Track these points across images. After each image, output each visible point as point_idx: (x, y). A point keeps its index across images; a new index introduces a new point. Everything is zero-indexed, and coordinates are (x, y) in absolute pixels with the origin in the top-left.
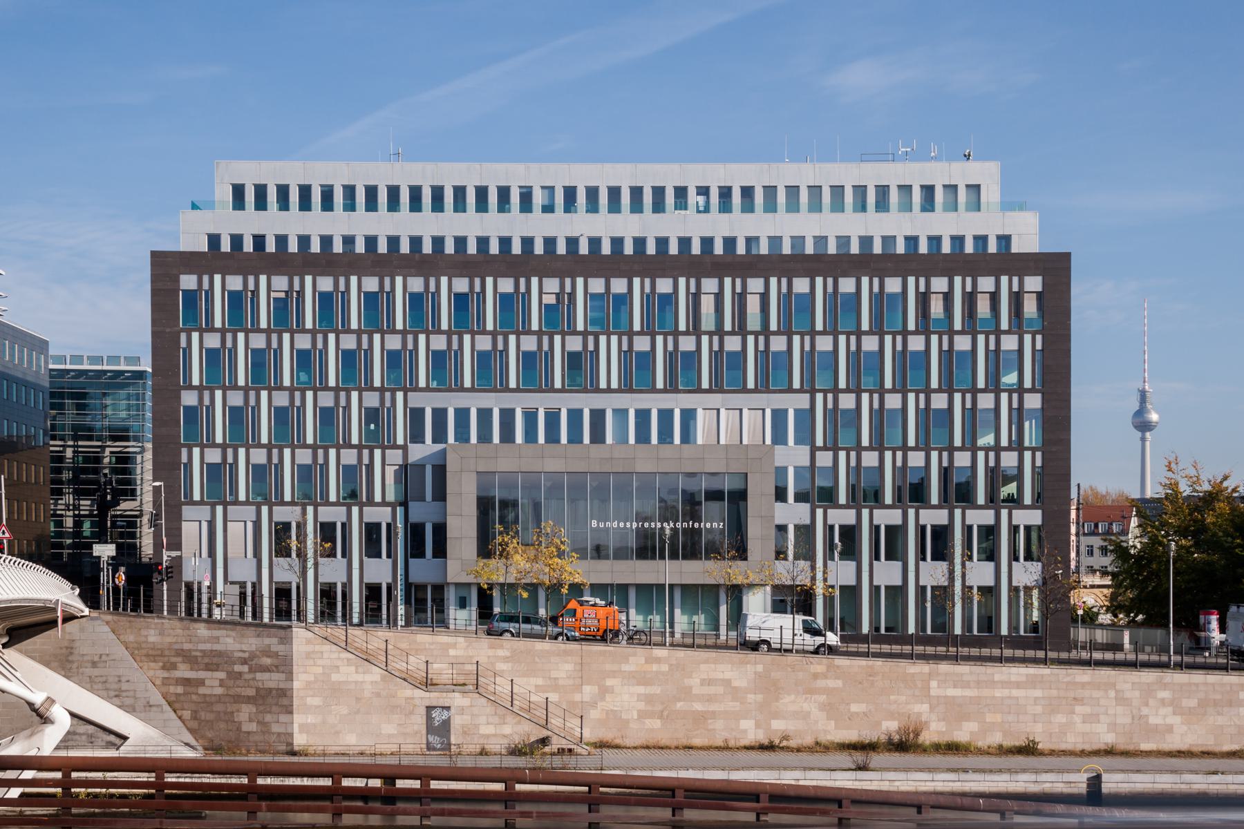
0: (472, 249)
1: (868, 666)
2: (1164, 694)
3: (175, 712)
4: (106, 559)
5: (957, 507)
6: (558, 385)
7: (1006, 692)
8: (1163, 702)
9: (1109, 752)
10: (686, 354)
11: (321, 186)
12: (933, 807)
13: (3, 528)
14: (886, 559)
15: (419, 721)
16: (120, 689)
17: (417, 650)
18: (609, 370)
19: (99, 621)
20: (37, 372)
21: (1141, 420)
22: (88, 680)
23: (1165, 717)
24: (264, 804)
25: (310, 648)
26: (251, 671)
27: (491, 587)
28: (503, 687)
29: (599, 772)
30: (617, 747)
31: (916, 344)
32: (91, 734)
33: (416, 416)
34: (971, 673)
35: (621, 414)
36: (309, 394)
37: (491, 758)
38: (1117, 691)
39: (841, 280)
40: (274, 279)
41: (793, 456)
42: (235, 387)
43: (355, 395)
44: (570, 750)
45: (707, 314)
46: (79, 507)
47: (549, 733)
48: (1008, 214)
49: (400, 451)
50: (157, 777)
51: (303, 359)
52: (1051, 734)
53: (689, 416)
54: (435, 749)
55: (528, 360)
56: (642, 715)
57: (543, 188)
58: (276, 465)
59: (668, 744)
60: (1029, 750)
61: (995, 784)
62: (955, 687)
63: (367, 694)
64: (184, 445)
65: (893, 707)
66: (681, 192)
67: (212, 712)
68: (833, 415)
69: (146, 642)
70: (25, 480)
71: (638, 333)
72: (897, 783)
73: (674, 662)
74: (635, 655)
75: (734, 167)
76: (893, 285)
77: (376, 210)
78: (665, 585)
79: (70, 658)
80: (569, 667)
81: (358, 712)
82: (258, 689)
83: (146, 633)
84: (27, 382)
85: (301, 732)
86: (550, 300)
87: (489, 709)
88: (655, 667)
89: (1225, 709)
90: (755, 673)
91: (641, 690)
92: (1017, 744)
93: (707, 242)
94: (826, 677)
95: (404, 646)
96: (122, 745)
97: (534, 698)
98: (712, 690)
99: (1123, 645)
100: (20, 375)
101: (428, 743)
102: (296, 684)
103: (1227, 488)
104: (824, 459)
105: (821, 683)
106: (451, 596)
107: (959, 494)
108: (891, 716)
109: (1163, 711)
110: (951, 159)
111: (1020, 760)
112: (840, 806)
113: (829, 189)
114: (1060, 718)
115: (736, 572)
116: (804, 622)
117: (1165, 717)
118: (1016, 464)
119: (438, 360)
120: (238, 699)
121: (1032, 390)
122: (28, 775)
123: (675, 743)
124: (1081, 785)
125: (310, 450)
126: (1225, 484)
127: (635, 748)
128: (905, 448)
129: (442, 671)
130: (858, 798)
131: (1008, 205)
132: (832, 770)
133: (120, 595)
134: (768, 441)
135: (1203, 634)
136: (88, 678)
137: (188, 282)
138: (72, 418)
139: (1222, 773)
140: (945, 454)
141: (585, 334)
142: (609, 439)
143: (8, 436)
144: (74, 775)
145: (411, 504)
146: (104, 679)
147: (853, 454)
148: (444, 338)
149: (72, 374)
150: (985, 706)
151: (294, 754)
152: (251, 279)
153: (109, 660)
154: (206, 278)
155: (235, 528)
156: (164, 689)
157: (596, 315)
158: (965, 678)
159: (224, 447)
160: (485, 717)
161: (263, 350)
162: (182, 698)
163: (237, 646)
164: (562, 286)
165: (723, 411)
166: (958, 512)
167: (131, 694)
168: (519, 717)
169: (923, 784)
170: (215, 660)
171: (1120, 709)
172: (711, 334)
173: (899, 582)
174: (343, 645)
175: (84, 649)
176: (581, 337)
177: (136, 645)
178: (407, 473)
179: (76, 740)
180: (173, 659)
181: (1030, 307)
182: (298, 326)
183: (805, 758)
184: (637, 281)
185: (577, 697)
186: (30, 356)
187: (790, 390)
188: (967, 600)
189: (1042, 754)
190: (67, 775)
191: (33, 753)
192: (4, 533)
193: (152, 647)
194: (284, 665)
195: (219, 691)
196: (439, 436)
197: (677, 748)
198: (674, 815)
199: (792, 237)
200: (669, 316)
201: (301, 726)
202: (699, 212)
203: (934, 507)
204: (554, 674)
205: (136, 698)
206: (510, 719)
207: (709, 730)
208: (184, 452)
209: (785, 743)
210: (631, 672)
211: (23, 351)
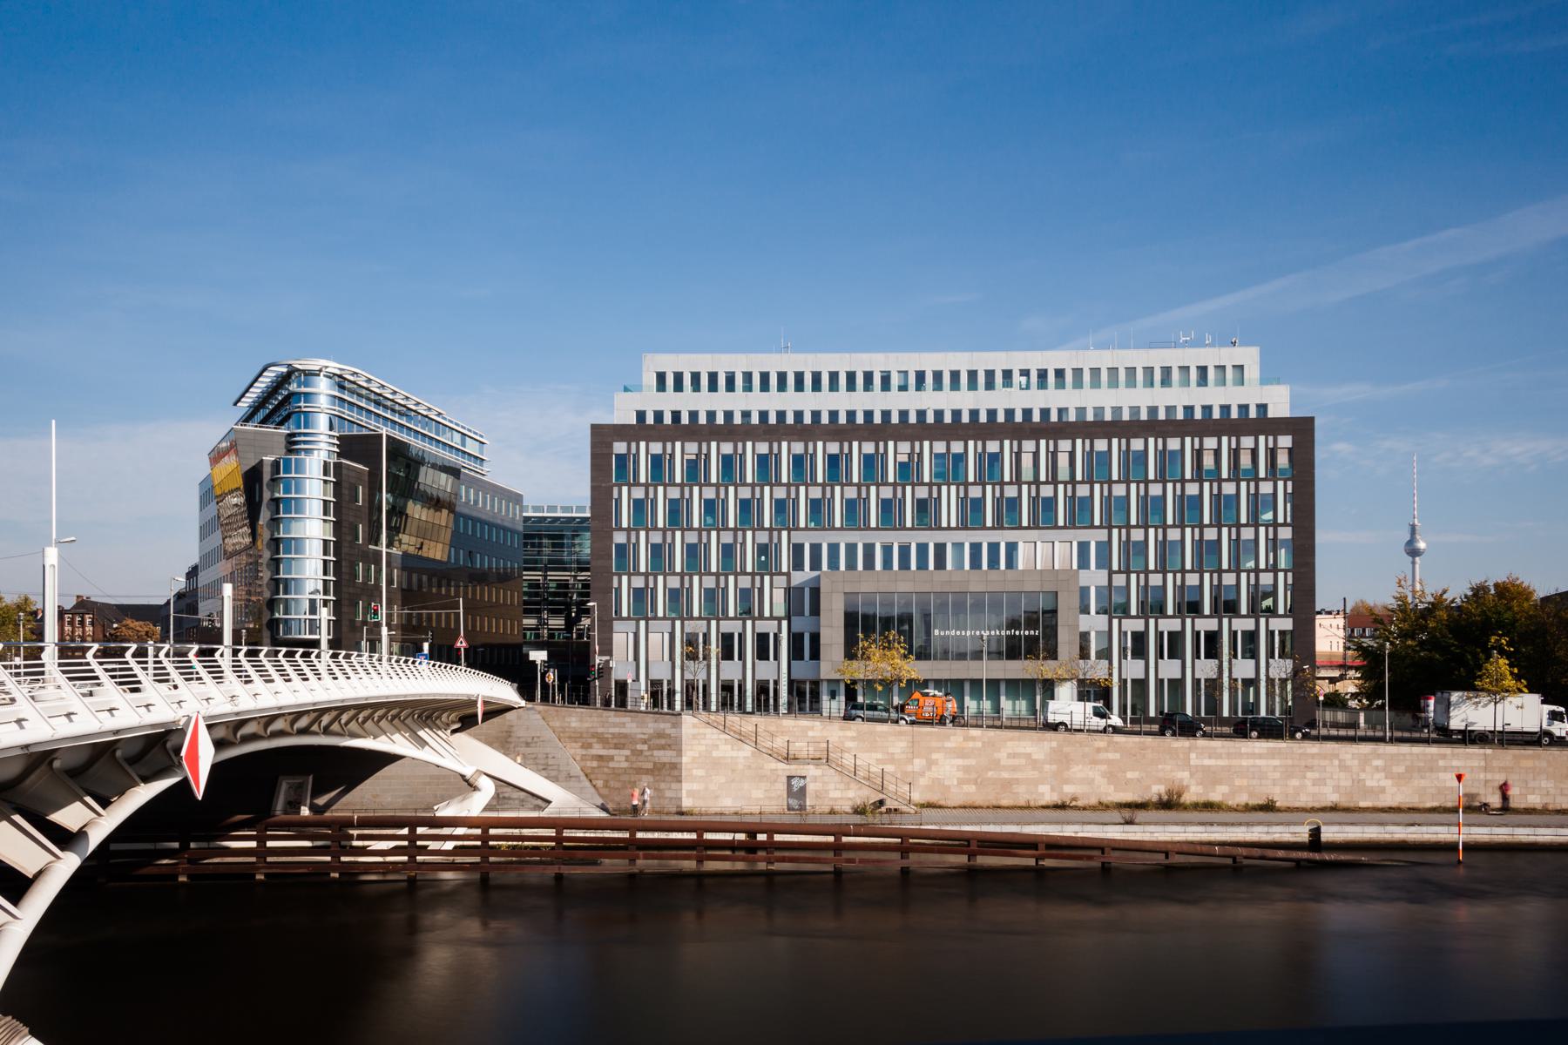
0: (842, 420)
1: (1140, 742)
2: (1378, 763)
3: (591, 781)
5: (1225, 617)
6: (909, 524)
7: (1251, 762)
8: (1377, 769)
9: (1334, 809)
10: (1046, 500)
11: (726, 373)
12: (1178, 853)
14: (1169, 658)
15: (781, 787)
17: (783, 732)
18: (949, 511)
20: (513, 519)
21: (1411, 548)
23: (1379, 780)
24: (641, 853)
25: (695, 731)
26: (649, 749)
27: (854, 682)
28: (848, 761)
29: (918, 827)
30: (940, 807)
31: (1192, 489)
33: (797, 550)
34: (1223, 747)
35: (959, 546)
36: (714, 534)
37: (838, 817)
38: (1340, 761)
39: (988, 443)
40: (687, 445)
41: (1094, 578)
42: (656, 529)
43: (749, 534)
44: (896, 810)
45: (1027, 468)
47: (884, 797)
48: (1265, 387)
49: (785, 577)
50: (630, 835)
51: (710, 507)
52: (1287, 795)
53: (1012, 548)
54: (793, 810)
55: (886, 506)
56: (961, 782)
57: (899, 372)
58: (687, 589)
59: (981, 804)
60: (1269, 807)
61: (1235, 835)
62: (1210, 758)
63: (740, 767)
64: (616, 574)
65: (1161, 775)
66: (1007, 374)
67: (619, 781)
68: (1126, 545)
69: (569, 727)
71: (972, 484)
72: (1156, 835)
73: (986, 740)
74: (955, 735)
75: (1049, 354)
76: (1174, 444)
77: (768, 391)
78: (982, 680)
79: (509, 740)
80: (903, 744)
81: (733, 781)
82: (655, 764)
85: (688, 796)
86: (903, 458)
87: (837, 778)
88: (971, 744)
89: (1427, 774)
90: (1051, 748)
91: (960, 762)
92: (1261, 802)
93: (1225, 409)
94: (1107, 751)
95: (772, 729)
97: (873, 769)
98: (1016, 762)
99: (1359, 724)
100: (499, 522)
101: (788, 805)
102: (684, 759)
103: (1446, 600)
104: (1119, 580)
105: (1103, 756)
106: (824, 688)
107: (1226, 607)
108: (1159, 781)
109: (1377, 776)
110: (1222, 345)
111: (1261, 815)
112: (1103, 853)
113: (1071, 371)
114: (1295, 782)
115: (1047, 669)
116: (1095, 708)
117: (1379, 780)
118: (1272, 582)
119: (815, 506)
120: (639, 771)
121: (1285, 524)
122: (460, 831)
123: (986, 804)
124: (1303, 835)
125: (714, 577)
126: (1445, 596)
127: (954, 808)
128: (1183, 571)
129: (800, 747)
130: (1117, 846)
131: (1265, 380)
132: (1106, 824)
134: (1075, 566)
135: (1423, 715)
137: (620, 447)
139: (1419, 825)
140: (1215, 575)
141: (930, 485)
142: (949, 566)
144: (492, 832)
145: (793, 618)
146: (533, 756)
147: (1142, 576)
148: (749, 489)
150: (1235, 772)
151: (682, 813)
152: (669, 445)
154: (846, 445)
155: (655, 638)
156: (583, 764)
157: (939, 470)
158: (1218, 751)
159: (646, 575)
160: (833, 785)
161: (642, 500)
162: (596, 771)
163: (639, 730)
164: (913, 448)
165: (1038, 543)
166: (1225, 621)
168: (860, 785)
169: (1177, 835)
170: (623, 741)
171: (1342, 775)
172: (1029, 484)
173: (1179, 676)
174: (722, 728)
175: (520, 732)
176: (927, 487)
177: (560, 729)
178: (793, 594)
180: (590, 741)
181: (1283, 460)
182: (705, 481)
183: (1088, 815)
184: (971, 443)
185: (909, 768)
187: (1092, 526)
188: (1233, 690)
189: (1279, 810)
190: (485, 831)
192: (461, 642)
194: (675, 744)
195: (625, 765)
196: (816, 565)
197: (988, 807)
198: (969, 860)
199: (1094, 408)
200: (961, 471)
201: (688, 791)
202: (1021, 389)
203: (1207, 617)
204: (891, 750)
205: (559, 771)
206: (853, 785)
207: (1014, 793)
208: (615, 579)
209: (1074, 803)
210: (950, 748)
211: (501, 503)
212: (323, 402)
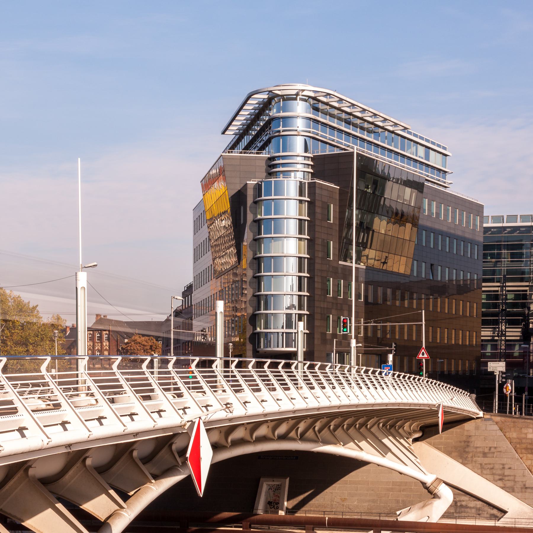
4: (498, 373)
13: (423, 351)
16: (504, 474)
19: (491, 421)
20: (474, 230)
22: (479, 467)
32: (479, 508)
46: (505, 334)
69: (526, 438)
70: (461, 314)
79: (467, 450)
83: (526, 431)
84: (465, 238)
96: (502, 517)
133: (507, 401)
136: (480, 465)
138: (507, 264)
143: (449, 280)
146: (491, 466)
149: (508, 230)
153: (496, 452)
167: (512, 478)
175: (478, 443)
177: (518, 441)
179: (468, 512)
186: (468, 218)
191: (424, 520)
193: (530, 442)
205: (515, 482)
212: (300, 125)
